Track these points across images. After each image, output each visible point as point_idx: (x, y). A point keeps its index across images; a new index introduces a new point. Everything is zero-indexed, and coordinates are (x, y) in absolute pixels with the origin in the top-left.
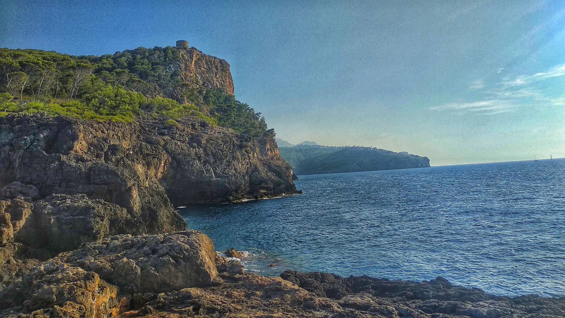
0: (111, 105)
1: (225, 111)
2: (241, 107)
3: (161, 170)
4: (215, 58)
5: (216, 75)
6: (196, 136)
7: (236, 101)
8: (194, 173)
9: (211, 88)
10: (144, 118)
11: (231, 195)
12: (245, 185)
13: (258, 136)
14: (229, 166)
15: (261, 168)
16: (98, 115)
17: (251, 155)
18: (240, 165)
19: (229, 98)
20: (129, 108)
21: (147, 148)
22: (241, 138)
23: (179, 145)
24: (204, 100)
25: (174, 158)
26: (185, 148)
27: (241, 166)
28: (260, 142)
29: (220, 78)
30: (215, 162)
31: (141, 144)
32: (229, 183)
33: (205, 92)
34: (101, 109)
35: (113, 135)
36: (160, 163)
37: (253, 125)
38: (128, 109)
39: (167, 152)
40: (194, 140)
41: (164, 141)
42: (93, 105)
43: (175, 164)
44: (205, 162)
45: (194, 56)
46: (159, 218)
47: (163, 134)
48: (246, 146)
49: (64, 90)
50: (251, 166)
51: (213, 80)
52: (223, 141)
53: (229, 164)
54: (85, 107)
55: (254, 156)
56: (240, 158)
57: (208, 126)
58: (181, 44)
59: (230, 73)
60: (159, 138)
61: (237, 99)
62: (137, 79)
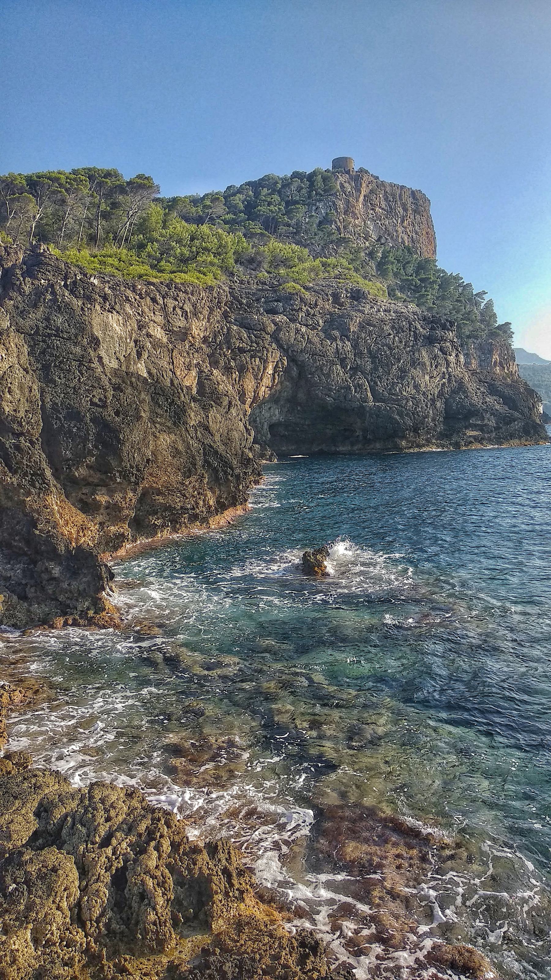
0: (182, 254)
1: (417, 289)
2: (447, 282)
3: (267, 381)
4: (403, 187)
5: (403, 222)
6: (340, 317)
7: (439, 270)
8: (330, 390)
9: (393, 247)
10: (242, 282)
11: (403, 437)
12: (434, 420)
13: (476, 337)
14: (402, 378)
15: (471, 386)
16: (154, 272)
17: (452, 358)
18: (427, 377)
19: (424, 265)
20: (216, 261)
21: (241, 337)
22: (432, 322)
23: (302, 333)
24: (378, 270)
25: (292, 360)
26: (316, 340)
27: (429, 381)
28: (480, 348)
29: (411, 228)
30: (376, 369)
31: (229, 329)
32: (400, 414)
33: (380, 255)
34: (163, 263)
35: (174, 309)
36: (265, 369)
37: (468, 316)
38: (212, 264)
39: (280, 346)
40: (335, 325)
41: (276, 324)
42: (149, 256)
43: (295, 371)
44: (355, 369)
45: (364, 185)
46: (126, 448)
47: (273, 312)
48: (443, 339)
49: (111, 235)
50: (449, 380)
51: (397, 231)
52: (393, 328)
53: (403, 373)
54: (134, 258)
55: (458, 361)
56: (428, 363)
57: (365, 298)
58: (341, 164)
59: (429, 217)
60: (266, 319)
61: (440, 265)
62: (259, 231)
